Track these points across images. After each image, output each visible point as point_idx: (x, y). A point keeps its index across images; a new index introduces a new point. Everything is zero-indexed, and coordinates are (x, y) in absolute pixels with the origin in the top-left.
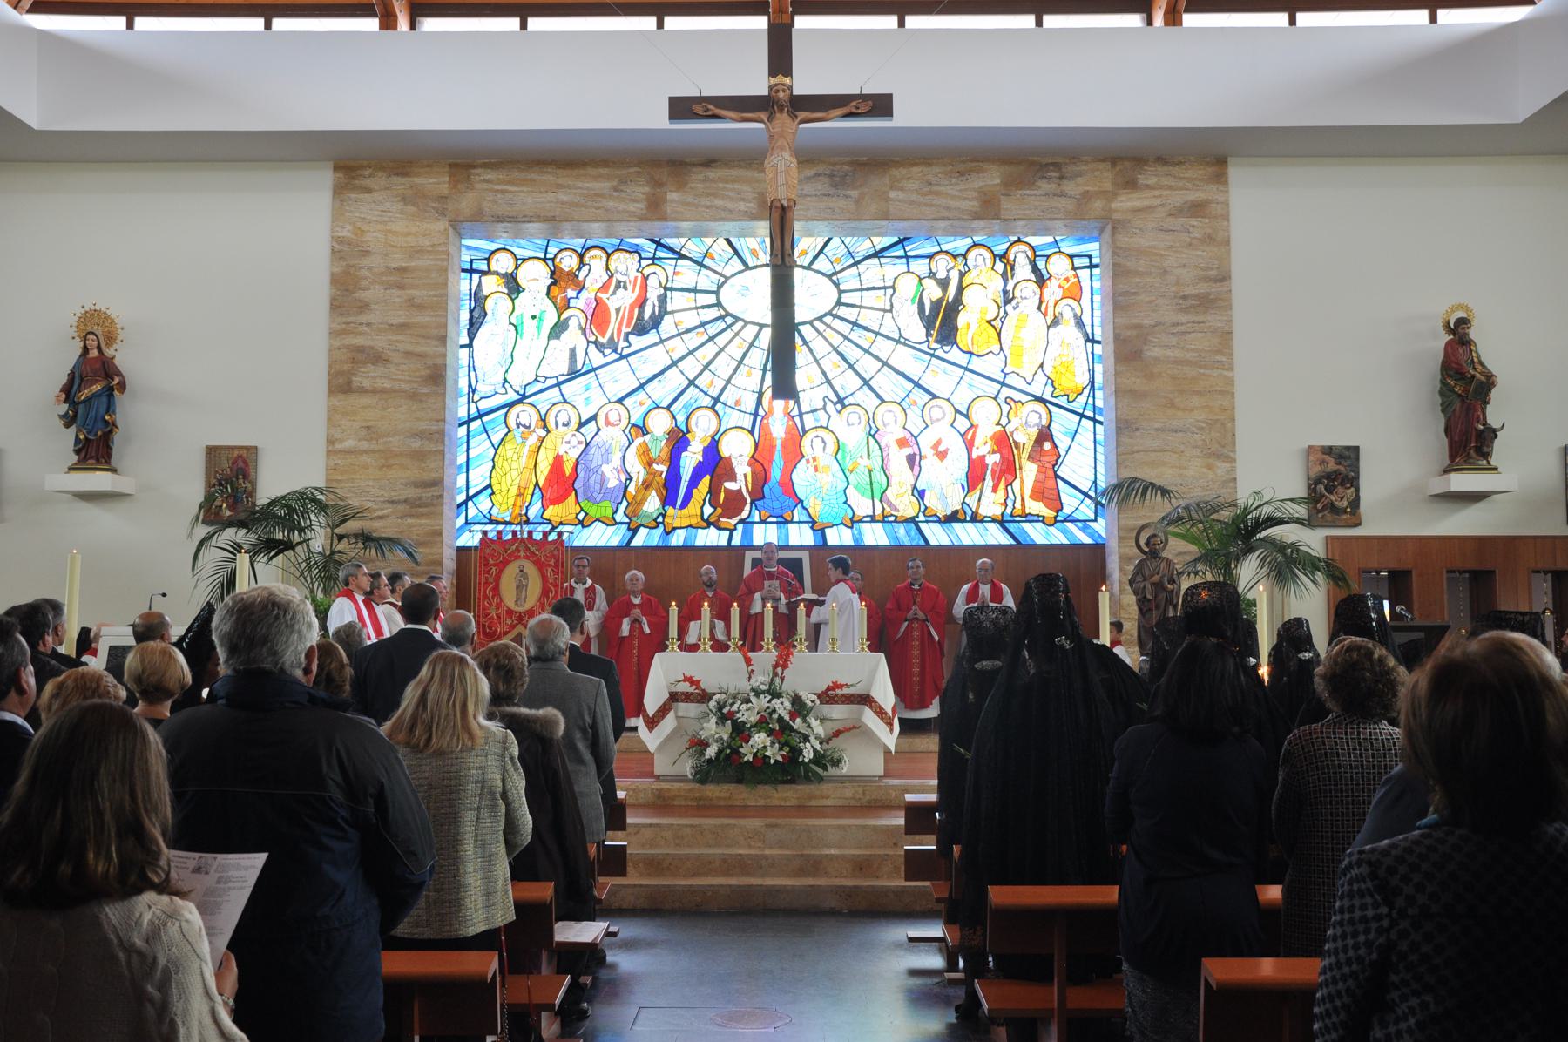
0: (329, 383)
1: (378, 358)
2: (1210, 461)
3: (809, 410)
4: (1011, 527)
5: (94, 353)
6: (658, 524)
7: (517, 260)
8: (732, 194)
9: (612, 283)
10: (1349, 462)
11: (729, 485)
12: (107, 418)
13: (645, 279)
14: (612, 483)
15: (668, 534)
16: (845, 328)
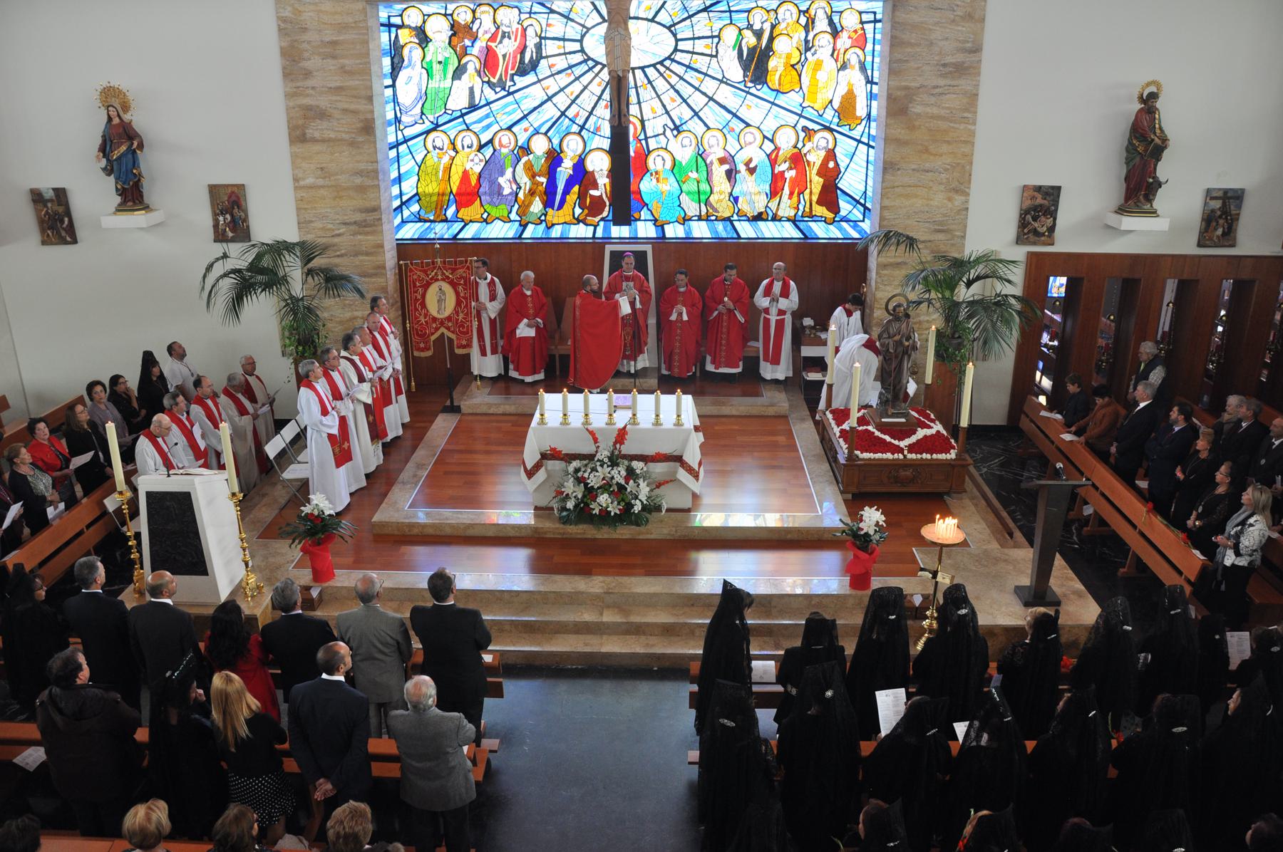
0: (289, 134)
1: (322, 115)
2: (950, 194)
3: (652, 135)
4: (802, 225)
5: (116, 121)
6: (542, 221)
7: (424, 15)
9: (498, 34)
10: (1052, 197)
11: (593, 192)
12: (134, 171)
13: (524, 30)
15: (549, 228)
16: (680, 70)
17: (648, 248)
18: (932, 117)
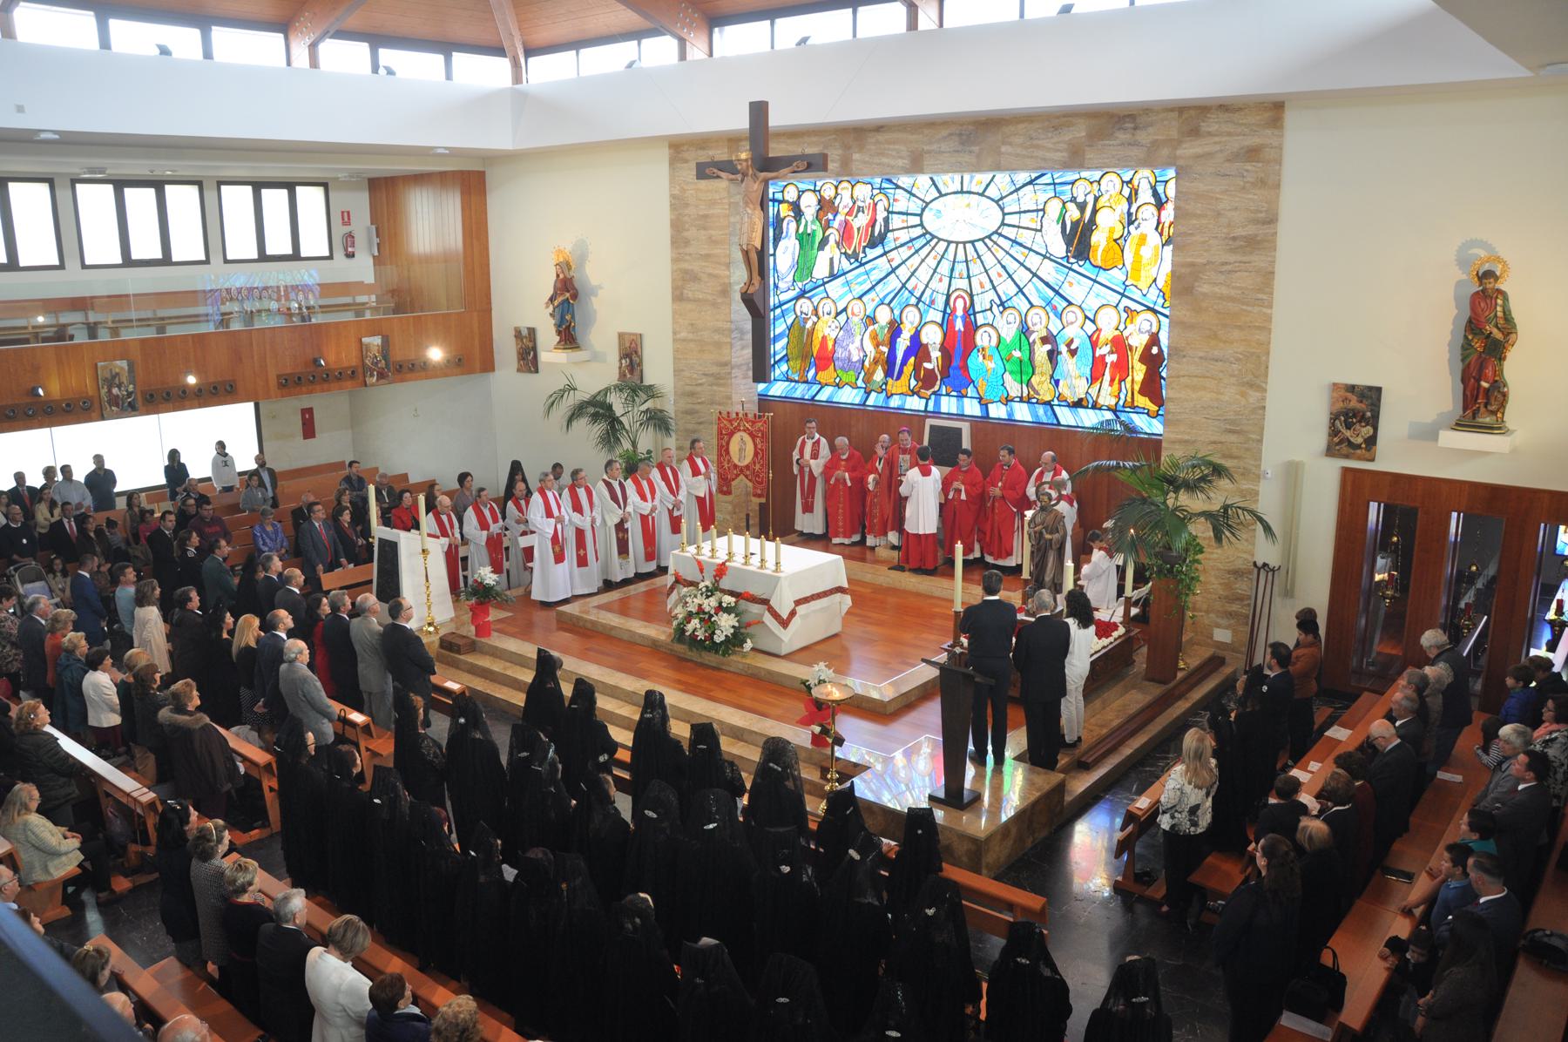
2: (1244, 389)
8: (894, 153)
9: (855, 210)
11: (927, 365)
13: (875, 205)
14: (855, 358)
15: (888, 398)
16: (1006, 244)
17: (965, 428)
18: (1220, 298)
